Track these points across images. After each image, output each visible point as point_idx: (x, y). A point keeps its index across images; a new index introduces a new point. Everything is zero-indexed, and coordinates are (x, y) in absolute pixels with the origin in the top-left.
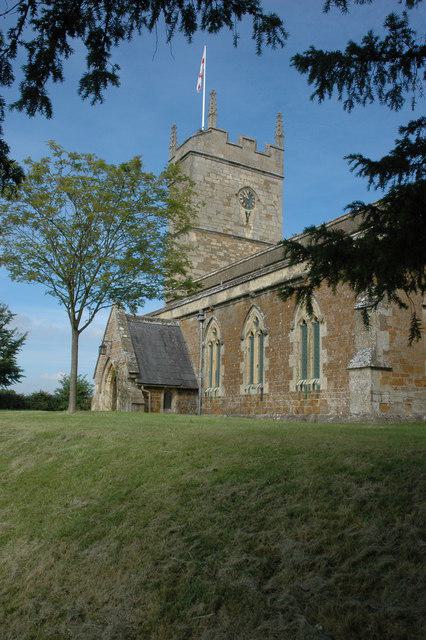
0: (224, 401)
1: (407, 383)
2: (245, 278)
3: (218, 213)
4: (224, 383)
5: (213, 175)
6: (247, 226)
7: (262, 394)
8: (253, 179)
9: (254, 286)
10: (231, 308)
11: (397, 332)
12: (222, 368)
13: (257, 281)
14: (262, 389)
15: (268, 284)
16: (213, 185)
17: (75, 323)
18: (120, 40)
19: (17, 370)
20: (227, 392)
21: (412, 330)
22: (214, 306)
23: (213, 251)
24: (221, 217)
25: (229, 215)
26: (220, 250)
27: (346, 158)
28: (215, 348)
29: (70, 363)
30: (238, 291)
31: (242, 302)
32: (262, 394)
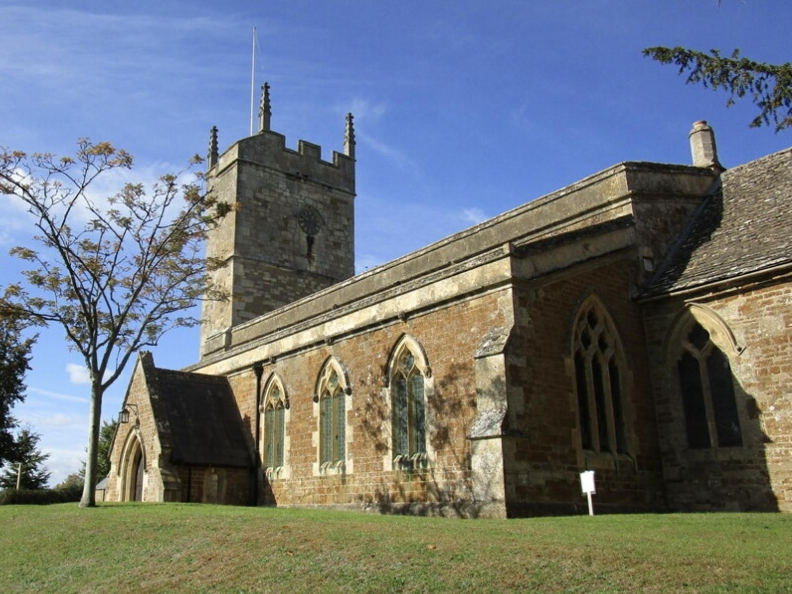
1: (549, 458)
2: (320, 319)
3: (272, 239)
5: (266, 192)
6: (309, 256)
7: (344, 475)
8: (316, 197)
10: (299, 357)
12: (254, 432)
13: (334, 322)
16: (265, 204)
18: (21, 287)
20: (295, 473)
23: (266, 288)
25: (286, 241)
26: (275, 287)
27: (687, 83)
28: (415, 443)
30: (307, 337)
31: (314, 352)
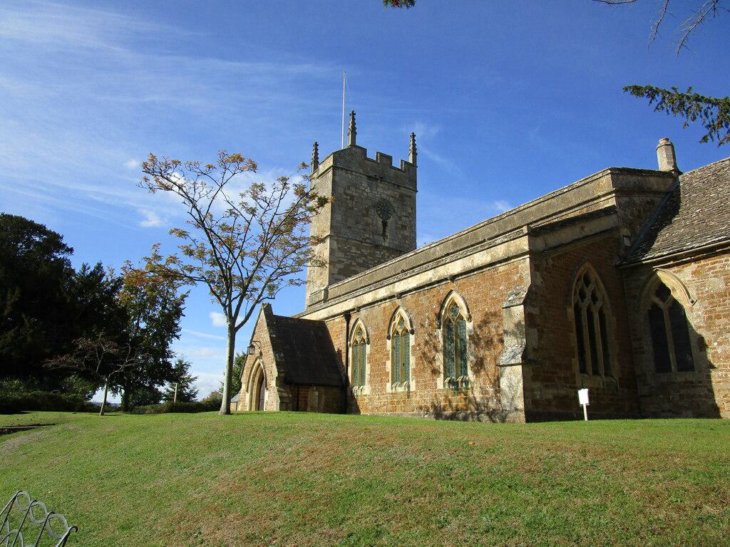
0: (370, 399)
4: (370, 382)
6: (384, 235)
7: (409, 392)
9: (400, 287)
11: (545, 330)
12: (344, 361)
14: (409, 387)
15: (414, 285)
16: (352, 198)
17: (232, 319)
19: (535, 381)
21: (452, 419)
22: (360, 308)
23: (353, 258)
24: (360, 226)
25: (367, 224)
29: (227, 359)
30: (382, 293)
31: (387, 303)
32: (409, 392)
